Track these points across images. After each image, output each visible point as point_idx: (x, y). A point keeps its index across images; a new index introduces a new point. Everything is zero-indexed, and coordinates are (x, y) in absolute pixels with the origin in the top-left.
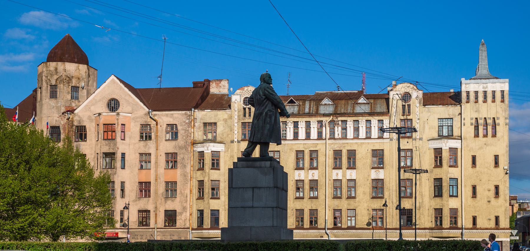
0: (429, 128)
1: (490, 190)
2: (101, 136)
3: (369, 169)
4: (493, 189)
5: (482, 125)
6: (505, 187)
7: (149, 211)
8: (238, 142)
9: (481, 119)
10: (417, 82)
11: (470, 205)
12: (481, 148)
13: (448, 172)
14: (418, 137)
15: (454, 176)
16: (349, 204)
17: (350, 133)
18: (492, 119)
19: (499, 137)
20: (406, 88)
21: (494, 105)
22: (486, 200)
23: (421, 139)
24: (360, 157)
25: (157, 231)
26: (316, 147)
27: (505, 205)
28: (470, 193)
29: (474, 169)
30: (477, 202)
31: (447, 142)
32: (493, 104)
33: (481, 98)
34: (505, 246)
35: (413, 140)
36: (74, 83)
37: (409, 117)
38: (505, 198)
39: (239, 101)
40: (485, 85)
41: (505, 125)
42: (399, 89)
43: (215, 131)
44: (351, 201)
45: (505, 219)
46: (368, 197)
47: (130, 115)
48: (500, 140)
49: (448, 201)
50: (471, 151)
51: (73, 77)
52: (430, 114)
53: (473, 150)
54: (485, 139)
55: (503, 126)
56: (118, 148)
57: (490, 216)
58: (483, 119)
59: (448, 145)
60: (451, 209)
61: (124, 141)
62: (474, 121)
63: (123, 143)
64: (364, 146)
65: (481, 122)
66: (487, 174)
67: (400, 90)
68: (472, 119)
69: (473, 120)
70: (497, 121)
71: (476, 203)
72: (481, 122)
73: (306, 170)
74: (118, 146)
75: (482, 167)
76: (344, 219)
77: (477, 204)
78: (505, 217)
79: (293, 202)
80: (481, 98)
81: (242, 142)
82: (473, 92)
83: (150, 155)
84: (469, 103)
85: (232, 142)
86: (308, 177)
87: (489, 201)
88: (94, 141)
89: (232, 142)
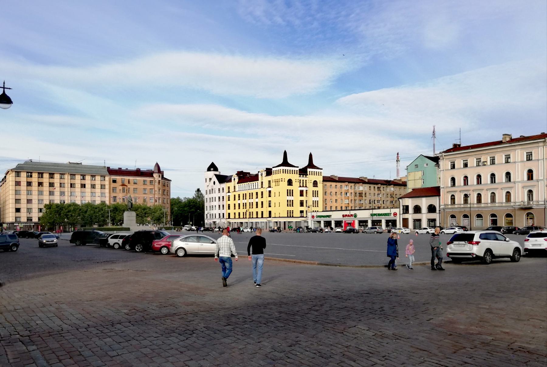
23: (265, 188)
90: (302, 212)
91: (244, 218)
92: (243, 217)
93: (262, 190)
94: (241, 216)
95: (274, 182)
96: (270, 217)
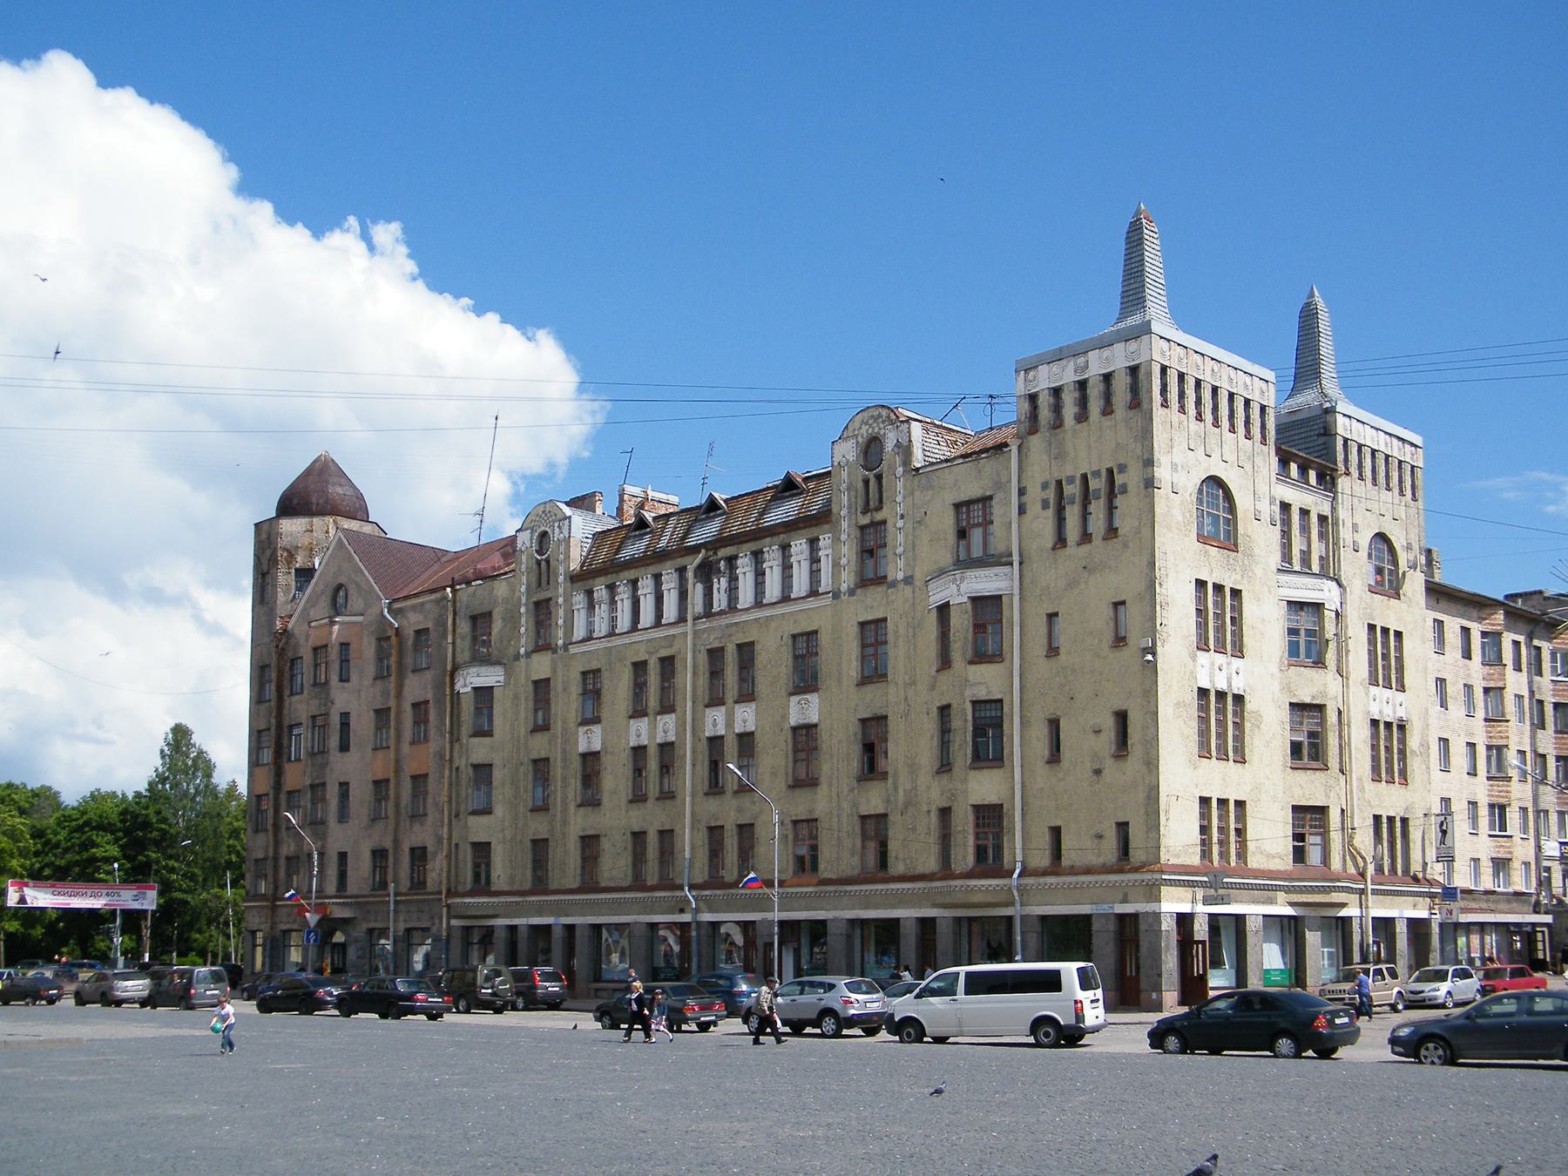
0: (931, 541)
1: (1100, 731)
2: (1332, 717)
3: (784, 694)
4: (1109, 723)
5: (1073, 503)
6: (1146, 713)
7: (387, 850)
8: (528, 655)
9: (1071, 480)
10: (991, 396)
11: (1042, 790)
12: (1072, 584)
13: (967, 681)
14: (900, 576)
15: (989, 693)
16: (740, 810)
17: (746, 596)
18: (1104, 473)
19: (1125, 535)
20: (870, 422)
21: (1109, 423)
22: (1088, 766)
23: (908, 580)
24: (765, 662)
25: (396, 902)
26: (671, 646)
27: (1147, 781)
28: (1042, 748)
29: (1053, 662)
30: (1061, 775)
31: (962, 579)
32: (1107, 422)
33: (1069, 410)
34: (1146, 931)
35: (889, 587)
36: (300, 561)
37: (879, 516)
38: (1148, 753)
39: (528, 545)
40: (1081, 360)
41: (1143, 486)
42: (854, 430)
43: (1149, 657)
44: (746, 800)
45: (1147, 832)
46: (781, 784)
47: (360, 619)
48: (1131, 545)
49: (965, 781)
50: (1043, 598)
51: (297, 547)
52: (930, 492)
53: (1049, 593)
54: (1086, 548)
55: (1138, 495)
56: (333, 703)
57: (1100, 822)
58: (1078, 482)
59: (964, 587)
60: (979, 809)
61: (346, 685)
62: (1051, 494)
63: (343, 688)
64: (773, 624)
65: (1072, 490)
66: (1091, 672)
67: (856, 432)
68: (1045, 486)
69: (1048, 491)
70: (1119, 479)
71: (1060, 780)
72: (1072, 490)
73: (651, 717)
74: (332, 696)
75: (1076, 651)
76: (730, 855)
77: (1062, 783)
78: (1147, 826)
79: (627, 812)
80: (1069, 410)
81: (535, 657)
82: (1046, 392)
83: (1296, 749)
84: (1038, 435)
85: (517, 657)
86: (655, 737)
87: (1098, 772)
88: (1431, 739)
89: (517, 657)
90: (1309, 818)
91: (638, 884)
92: (931, 863)
93: (872, 604)
94: (614, 864)
95: (1045, 504)
96: (989, 861)
